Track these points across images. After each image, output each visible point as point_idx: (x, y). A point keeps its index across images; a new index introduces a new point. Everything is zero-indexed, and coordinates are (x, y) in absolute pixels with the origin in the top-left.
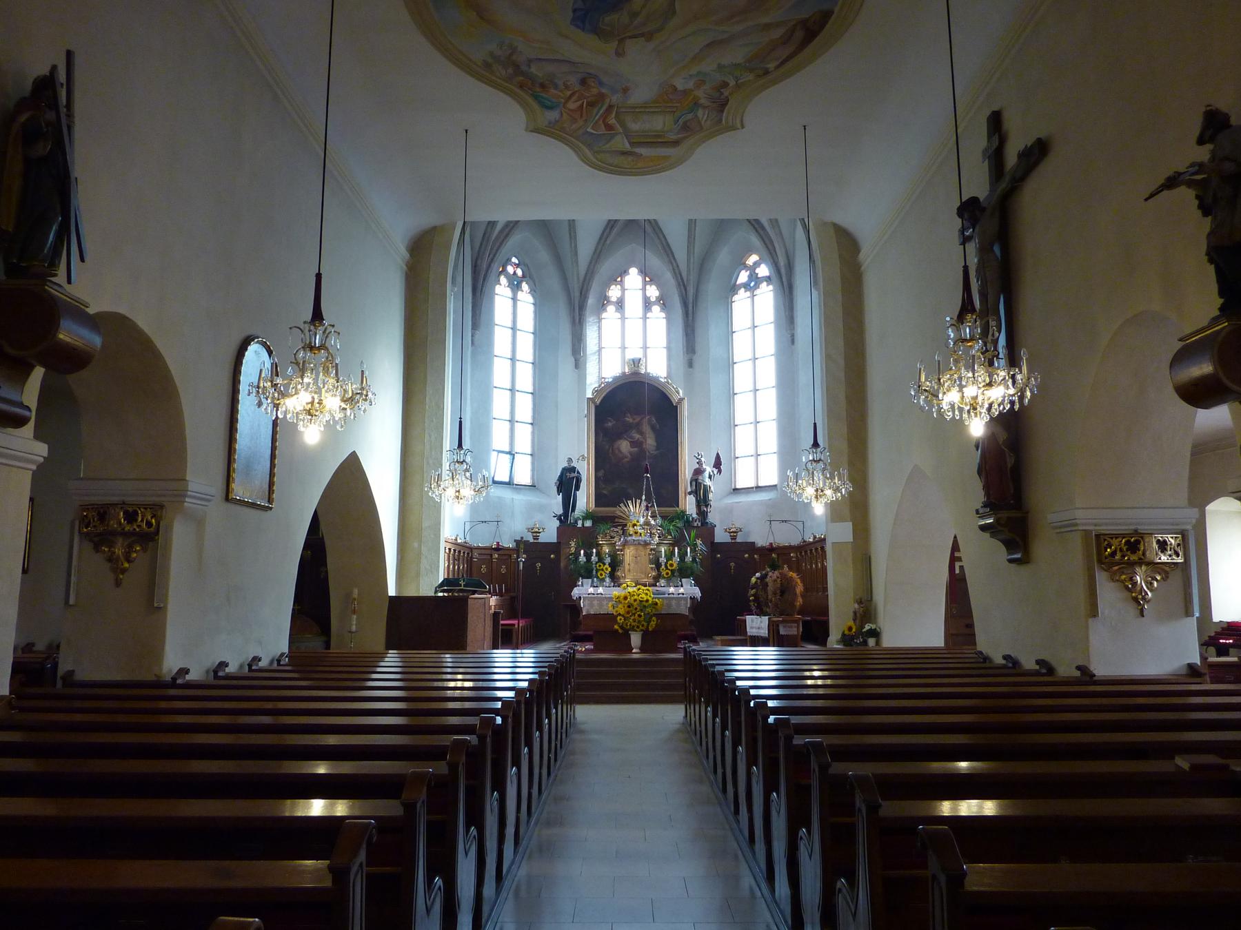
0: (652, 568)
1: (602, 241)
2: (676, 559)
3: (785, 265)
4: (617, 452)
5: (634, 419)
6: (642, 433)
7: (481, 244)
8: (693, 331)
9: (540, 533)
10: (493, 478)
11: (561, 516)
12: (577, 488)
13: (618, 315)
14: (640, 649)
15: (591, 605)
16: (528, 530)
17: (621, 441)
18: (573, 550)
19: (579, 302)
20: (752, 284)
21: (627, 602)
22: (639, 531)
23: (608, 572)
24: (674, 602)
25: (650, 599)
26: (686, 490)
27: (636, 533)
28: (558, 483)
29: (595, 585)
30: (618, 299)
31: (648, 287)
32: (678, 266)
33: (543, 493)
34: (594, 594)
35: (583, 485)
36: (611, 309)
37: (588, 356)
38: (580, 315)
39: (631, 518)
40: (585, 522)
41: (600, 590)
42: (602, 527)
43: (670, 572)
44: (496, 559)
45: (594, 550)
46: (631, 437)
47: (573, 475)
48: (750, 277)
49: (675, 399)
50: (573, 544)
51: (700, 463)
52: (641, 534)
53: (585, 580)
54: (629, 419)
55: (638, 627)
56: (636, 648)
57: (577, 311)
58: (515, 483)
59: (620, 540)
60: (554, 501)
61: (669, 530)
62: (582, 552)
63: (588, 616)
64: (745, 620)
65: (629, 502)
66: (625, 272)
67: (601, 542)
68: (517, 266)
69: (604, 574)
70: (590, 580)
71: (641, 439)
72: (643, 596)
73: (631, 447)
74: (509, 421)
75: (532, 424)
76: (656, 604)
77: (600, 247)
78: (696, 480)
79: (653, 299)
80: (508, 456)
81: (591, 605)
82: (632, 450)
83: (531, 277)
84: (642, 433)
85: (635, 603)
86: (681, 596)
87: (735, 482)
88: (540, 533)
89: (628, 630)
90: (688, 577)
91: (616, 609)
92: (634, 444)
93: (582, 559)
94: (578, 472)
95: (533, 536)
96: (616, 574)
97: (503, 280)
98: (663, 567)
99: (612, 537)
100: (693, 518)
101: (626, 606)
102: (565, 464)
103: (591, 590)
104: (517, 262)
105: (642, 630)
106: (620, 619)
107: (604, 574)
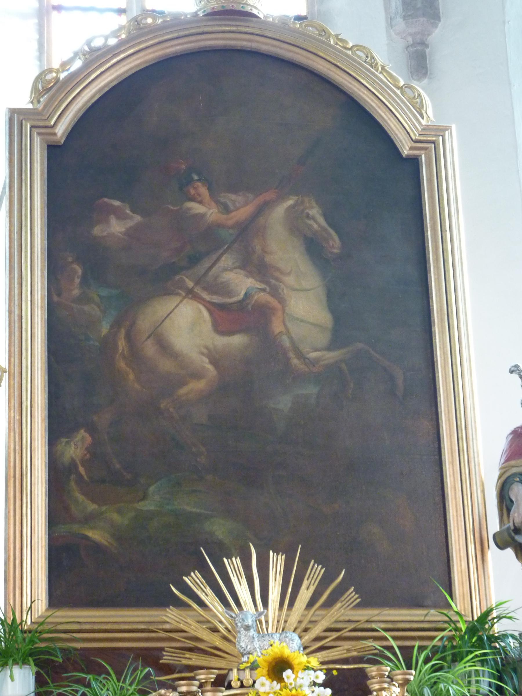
5: (226, 209)
17: (171, 302)
71: (264, 297)
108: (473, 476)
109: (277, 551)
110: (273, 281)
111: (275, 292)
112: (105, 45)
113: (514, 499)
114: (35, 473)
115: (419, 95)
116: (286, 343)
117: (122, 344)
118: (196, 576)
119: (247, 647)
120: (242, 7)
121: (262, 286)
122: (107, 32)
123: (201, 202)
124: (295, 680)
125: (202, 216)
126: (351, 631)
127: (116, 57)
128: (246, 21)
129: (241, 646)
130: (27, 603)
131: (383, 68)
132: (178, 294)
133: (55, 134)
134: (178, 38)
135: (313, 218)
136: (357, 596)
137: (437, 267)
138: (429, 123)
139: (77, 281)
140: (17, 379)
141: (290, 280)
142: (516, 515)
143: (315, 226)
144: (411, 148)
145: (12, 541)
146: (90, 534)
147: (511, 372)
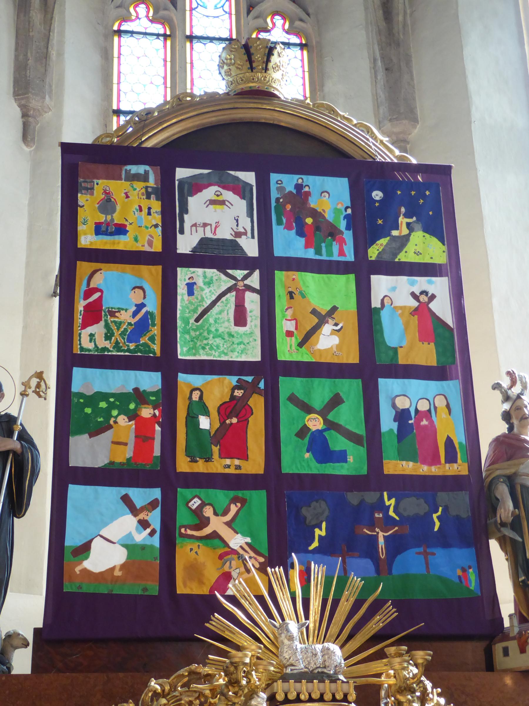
94: (24, 437)
113: (499, 497)
119: (290, 659)
120: (266, 88)
127: (161, 125)
129: (284, 657)
136: (394, 610)
142: (502, 510)
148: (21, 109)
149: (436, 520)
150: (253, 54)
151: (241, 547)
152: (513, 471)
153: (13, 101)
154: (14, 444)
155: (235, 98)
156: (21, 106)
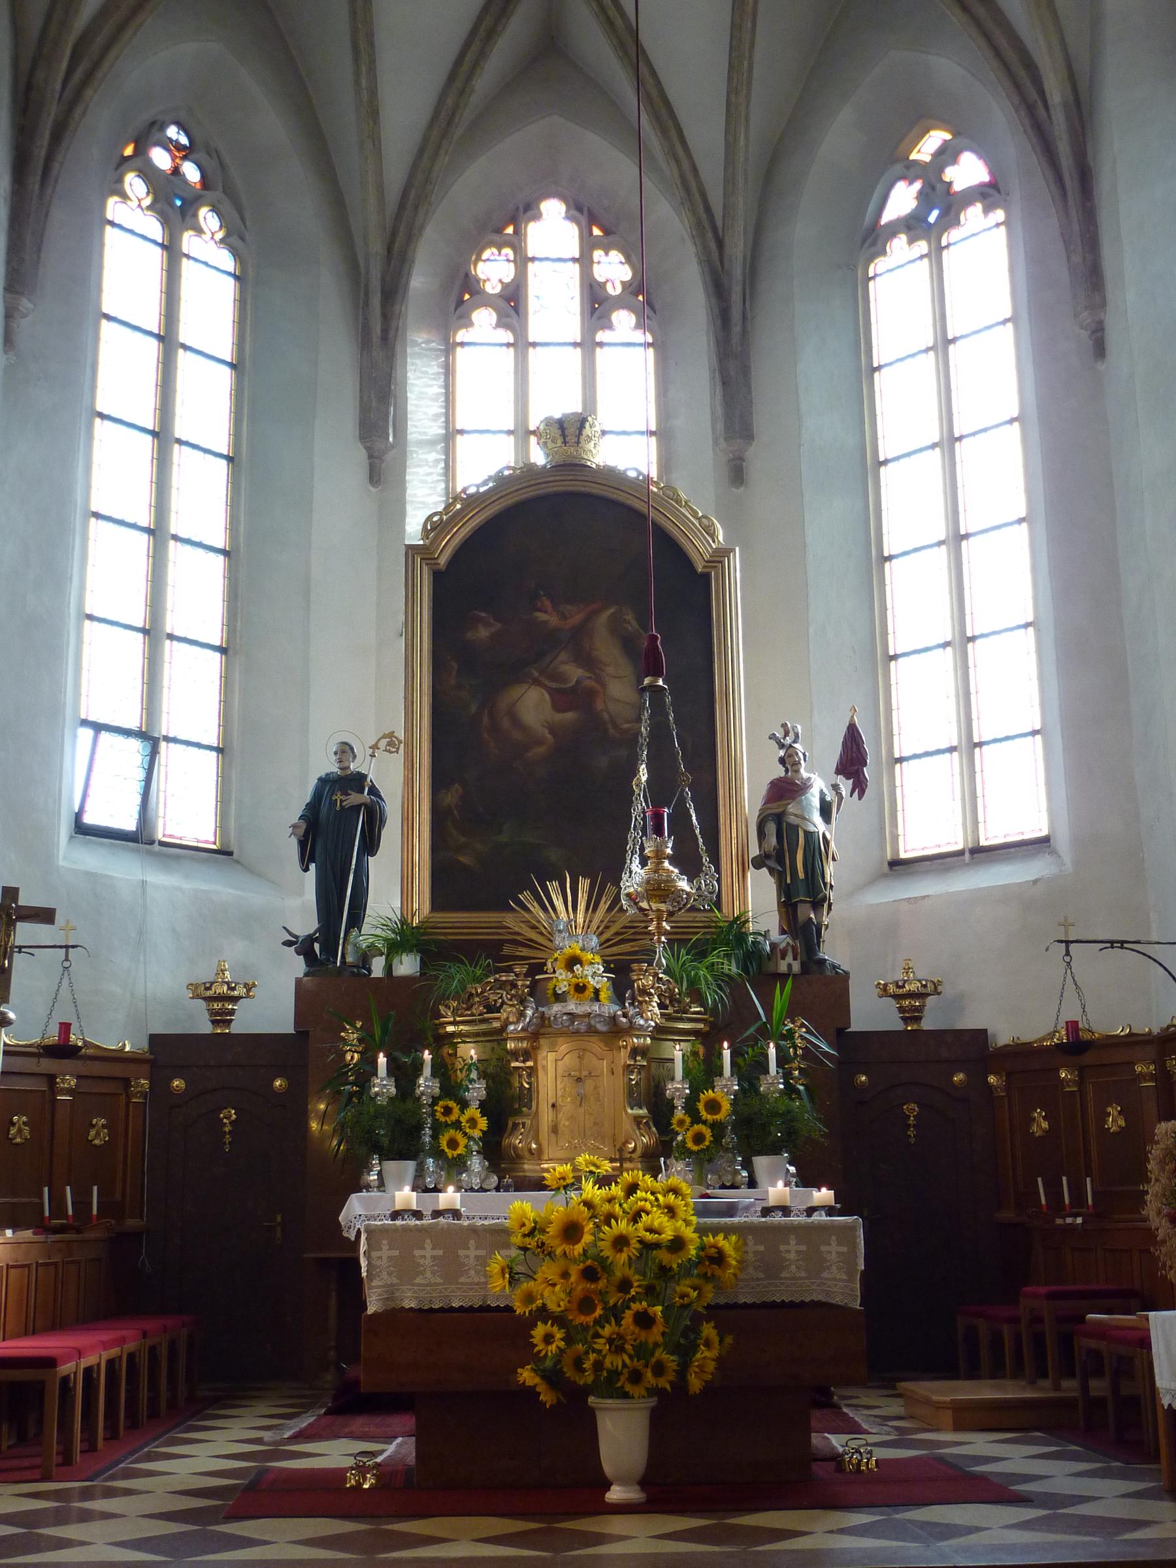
0: (637, 1120)
1: (458, 84)
2: (726, 1087)
3: (1065, 105)
4: (506, 723)
5: (564, 617)
6: (588, 661)
7: (49, 16)
8: (745, 371)
9: (235, 1000)
10: (78, 816)
11: (310, 939)
12: (371, 845)
13: (507, 336)
14: (644, 1483)
15: (406, 1268)
16: (193, 987)
18: (353, 1058)
19: (383, 280)
20: (933, 217)
21: (579, 1248)
22: (592, 982)
23: (477, 1134)
24: (792, 1249)
25: (689, 1233)
26: (744, 848)
27: (580, 989)
28: (304, 826)
29: (430, 1182)
30: (505, 286)
31: (598, 254)
32: (695, 170)
33: (259, 876)
34: (417, 1214)
35: (391, 835)
36: (484, 319)
37: (411, 448)
38: (388, 317)
39: (558, 940)
40: (395, 961)
41: (450, 1197)
42: (457, 975)
43: (708, 1133)
44: (69, 1091)
45: (427, 1055)
46: (559, 677)
47: (354, 798)
48: (926, 199)
49: (699, 550)
50: (351, 1035)
51: (789, 761)
52: (597, 992)
53: (391, 1166)
54: (548, 617)
55: (636, 1377)
56: (624, 1481)
57: (376, 301)
58: (160, 836)
59: (522, 1014)
60: (294, 903)
61: (693, 983)
62: (382, 1059)
63: (394, 1317)
64: (1145, 1343)
65: (553, 887)
66: (527, 210)
67: (450, 1029)
68: (187, 153)
69: (462, 1141)
70: (410, 1165)
72: (658, 1218)
73: (557, 708)
74: (143, 631)
75: (222, 650)
76: (719, 1258)
77: (450, 101)
78: (779, 818)
79: (614, 290)
80: (135, 744)
81: (406, 1268)
82: (559, 717)
83: (230, 192)
84: (588, 661)
85: (623, 1257)
86: (778, 1218)
87: (895, 838)
88: (235, 1000)
89: (586, 1391)
90: (774, 1150)
91: (527, 1285)
92: (564, 698)
93: (383, 1085)
94: (374, 791)
95: (213, 1013)
96: (506, 1142)
97: (134, 184)
98: (679, 1113)
99: (491, 1008)
100: (774, 946)
101: (575, 1271)
102: (329, 766)
103: (405, 1196)
104: (184, 140)
105: (652, 1392)
106: (548, 1339)
107: (462, 1141)
108: (739, 816)
109: (584, 877)
110: (598, 671)
111: (599, 680)
112: (478, 492)
114: (422, 816)
115: (713, 524)
116: (606, 716)
117: (486, 720)
118: (527, 893)
121: (590, 675)
122: (479, 481)
123: (545, 612)
124: (582, 972)
125: (546, 622)
126: (633, 934)
128: (581, 471)
130: (416, 906)
131: (686, 503)
132: (527, 682)
133: (439, 564)
134: (530, 486)
135: (629, 623)
137: (720, 658)
138: (720, 546)
139: (454, 673)
140: (410, 748)
141: (610, 670)
143: (630, 628)
144: (704, 567)
145: (406, 864)
146: (461, 859)
147: (770, 739)
148: (367, 451)
149: (671, 868)
150: (566, 429)
151: (232, 1012)
152: (781, 810)
153: (359, 444)
154: (366, 796)
155: (553, 471)
156: (367, 449)
